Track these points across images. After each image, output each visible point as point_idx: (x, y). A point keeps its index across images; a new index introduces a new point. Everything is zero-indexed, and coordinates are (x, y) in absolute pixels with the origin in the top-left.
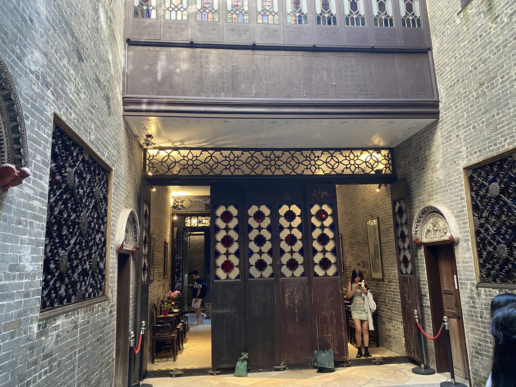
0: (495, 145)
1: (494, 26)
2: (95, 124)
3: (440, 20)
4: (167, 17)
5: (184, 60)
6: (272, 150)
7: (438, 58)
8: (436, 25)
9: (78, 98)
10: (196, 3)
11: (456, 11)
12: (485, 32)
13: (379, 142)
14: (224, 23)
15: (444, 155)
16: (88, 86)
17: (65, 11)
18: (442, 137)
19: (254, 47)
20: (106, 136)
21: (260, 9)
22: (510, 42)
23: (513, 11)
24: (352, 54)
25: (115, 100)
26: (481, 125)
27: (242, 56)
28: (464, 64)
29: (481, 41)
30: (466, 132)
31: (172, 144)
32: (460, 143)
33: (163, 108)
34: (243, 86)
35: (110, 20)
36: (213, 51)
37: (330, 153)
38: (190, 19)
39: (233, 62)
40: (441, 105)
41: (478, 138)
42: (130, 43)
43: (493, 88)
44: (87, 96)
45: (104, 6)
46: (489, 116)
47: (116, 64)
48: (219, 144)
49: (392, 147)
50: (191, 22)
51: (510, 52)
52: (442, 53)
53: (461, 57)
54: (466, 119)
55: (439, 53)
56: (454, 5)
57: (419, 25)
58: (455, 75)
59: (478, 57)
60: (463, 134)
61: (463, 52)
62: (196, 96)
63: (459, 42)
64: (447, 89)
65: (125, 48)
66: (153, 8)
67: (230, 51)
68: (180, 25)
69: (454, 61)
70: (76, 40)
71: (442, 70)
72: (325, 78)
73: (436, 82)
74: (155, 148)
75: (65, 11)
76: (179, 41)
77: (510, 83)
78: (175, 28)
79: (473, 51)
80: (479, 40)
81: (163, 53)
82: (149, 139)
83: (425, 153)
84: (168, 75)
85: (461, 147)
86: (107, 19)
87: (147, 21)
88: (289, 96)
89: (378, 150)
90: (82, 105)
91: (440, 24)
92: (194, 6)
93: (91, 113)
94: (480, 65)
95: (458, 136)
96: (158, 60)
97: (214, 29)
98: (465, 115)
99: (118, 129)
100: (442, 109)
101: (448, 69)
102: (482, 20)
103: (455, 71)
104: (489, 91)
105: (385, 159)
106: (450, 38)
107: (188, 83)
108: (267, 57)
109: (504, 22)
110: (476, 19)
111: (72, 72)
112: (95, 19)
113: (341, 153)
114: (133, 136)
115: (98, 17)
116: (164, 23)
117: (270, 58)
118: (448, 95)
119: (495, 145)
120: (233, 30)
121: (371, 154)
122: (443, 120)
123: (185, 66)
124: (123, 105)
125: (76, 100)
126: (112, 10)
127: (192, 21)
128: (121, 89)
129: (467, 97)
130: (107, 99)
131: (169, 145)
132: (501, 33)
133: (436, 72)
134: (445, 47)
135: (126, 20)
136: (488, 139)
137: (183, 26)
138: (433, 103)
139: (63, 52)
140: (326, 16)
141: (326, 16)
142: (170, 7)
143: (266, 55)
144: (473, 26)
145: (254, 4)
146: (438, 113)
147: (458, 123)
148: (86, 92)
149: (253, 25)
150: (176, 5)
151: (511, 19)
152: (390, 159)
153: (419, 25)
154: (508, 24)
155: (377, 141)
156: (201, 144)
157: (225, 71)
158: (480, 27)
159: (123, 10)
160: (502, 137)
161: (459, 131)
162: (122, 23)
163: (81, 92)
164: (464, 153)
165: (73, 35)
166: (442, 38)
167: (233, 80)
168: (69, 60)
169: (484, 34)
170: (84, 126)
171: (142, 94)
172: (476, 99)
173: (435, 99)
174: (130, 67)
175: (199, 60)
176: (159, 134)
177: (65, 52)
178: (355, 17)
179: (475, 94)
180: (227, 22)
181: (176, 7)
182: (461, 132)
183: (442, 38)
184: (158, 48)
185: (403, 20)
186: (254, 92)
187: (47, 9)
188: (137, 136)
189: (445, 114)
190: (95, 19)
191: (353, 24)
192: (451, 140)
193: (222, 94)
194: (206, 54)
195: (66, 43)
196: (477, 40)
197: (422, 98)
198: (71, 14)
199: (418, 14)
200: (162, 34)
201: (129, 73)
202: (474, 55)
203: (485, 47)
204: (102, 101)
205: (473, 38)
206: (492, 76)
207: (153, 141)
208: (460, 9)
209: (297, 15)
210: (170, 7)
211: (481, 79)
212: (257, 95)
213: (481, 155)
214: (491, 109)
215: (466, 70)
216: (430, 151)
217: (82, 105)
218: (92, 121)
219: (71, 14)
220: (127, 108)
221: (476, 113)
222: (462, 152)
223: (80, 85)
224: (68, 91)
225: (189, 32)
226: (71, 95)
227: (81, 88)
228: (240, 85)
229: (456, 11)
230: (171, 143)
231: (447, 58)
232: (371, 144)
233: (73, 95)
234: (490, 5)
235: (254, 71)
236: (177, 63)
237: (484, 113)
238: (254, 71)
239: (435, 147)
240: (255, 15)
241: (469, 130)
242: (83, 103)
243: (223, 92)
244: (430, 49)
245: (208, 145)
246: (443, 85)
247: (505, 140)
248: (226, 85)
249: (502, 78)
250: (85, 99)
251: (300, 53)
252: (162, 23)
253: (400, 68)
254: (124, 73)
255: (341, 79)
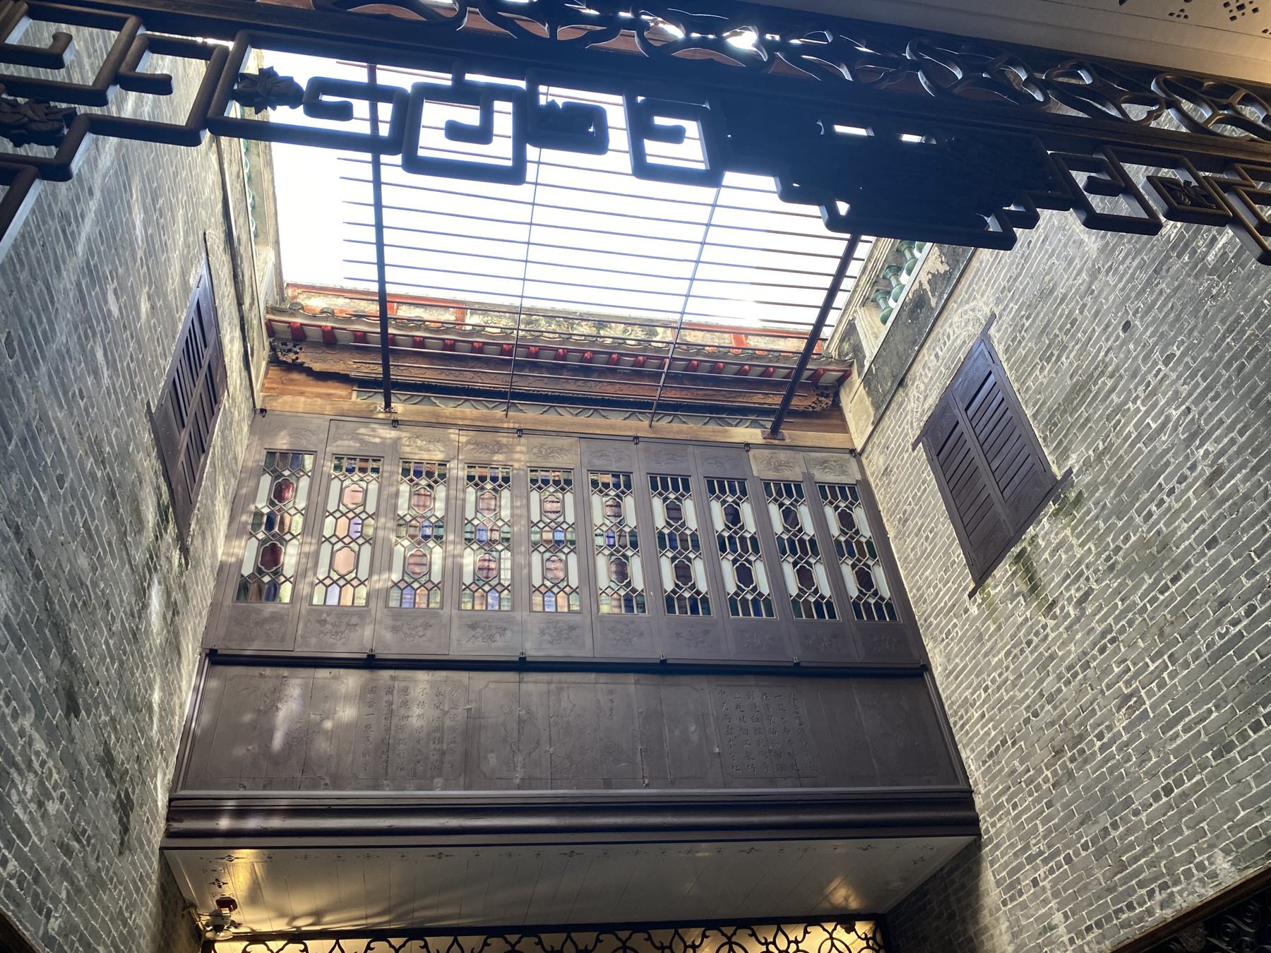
0: (1130, 907)
1: (1051, 623)
2: (72, 883)
3: (936, 606)
4: (317, 600)
5: (347, 698)
6: (568, 929)
7: (947, 688)
8: (929, 616)
9: (38, 816)
10: (390, 569)
11: (964, 590)
12: (1037, 634)
13: (846, 899)
14: (455, 612)
15: (1015, 936)
16: (76, 778)
17: (60, 600)
18: (998, 884)
19: (522, 666)
20: (95, 915)
21: (537, 581)
22: (1094, 658)
23: (1082, 593)
24: (751, 680)
25: (145, 808)
26: (1084, 854)
27: (492, 685)
28: (1007, 703)
29: (1032, 653)
30: (1051, 871)
31: (289, 924)
32: (1046, 902)
33: (276, 823)
34: (492, 759)
35: (173, 609)
36: (422, 676)
37: (723, 934)
38: (373, 605)
39: (469, 702)
40: (979, 802)
41: (1085, 888)
42: (215, 658)
43: (1086, 761)
44: (67, 806)
45: (164, 581)
46: (1096, 830)
47: (167, 710)
48: (423, 915)
49: (880, 912)
50: (373, 612)
51: (1100, 679)
52: (956, 678)
53: (999, 688)
54: (1045, 837)
55: (948, 676)
56: (958, 576)
57: (892, 616)
58: (995, 728)
59: (1034, 688)
60: (1046, 877)
61: (1000, 675)
62: (368, 788)
63: (986, 655)
64: (984, 762)
65: (200, 672)
66: (287, 580)
67: (463, 676)
68: (348, 617)
69: (983, 696)
70: (72, 664)
71: (962, 717)
72: (695, 738)
73: (956, 745)
74: (237, 938)
75: (60, 600)
76: (341, 650)
77: (1120, 749)
78: (334, 625)
79: (1020, 676)
80: (1027, 651)
81: (295, 684)
82: (226, 911)
83: (965, 931)
84: (302, 736)
85: (1049, 914)
86: (167, 607)
87: (269, 608)
88: (608, 784)
89: (847, 921)
90: (45, 832)
91: (937, 615)
92: (385, 576)
93: (68, 851)
94: (1042, 707)
95: (1035, 882)
96: (279, 699)
97: (427, 626)
98: (1040, 826)
99: (137, 890)
100: (982, 811)
101: (976, 715)
102: (1023, 611)
103: (991, 719)
104: (1079, 769)
105: (868, 947)
106: (966, 644)
107: (351, 756)
108: (553, 687)
109: (1068, 614)
110: (1010, 607)
111: (39, 745)
112: (136, 609)
113: (754, 934)
114: (181, 905)
115: (145, 606)
116: (309, 612)
117: (560, 690)
118: (990, 776)
119: (1130, 907)
120: (473, 627)
121: (831, 934)
122: (991, 840)
123: (347, 713)
124: (168, 820)
125: (33, 820)
126: (184, 588)
127: (377, 608)
128: (170, 776)
129: (1032, 781)
130: (125, 807)
131: (280, 925)
132: (1071, 639)
133: (951, 720)
134: (957, 665)
135: (215, 607)
136: (1110, 890)
137: (354, 620)
138: (957, 795)
139: (26, 696)
140: (687, 595)
141: (687, 595)
142: (360, 546)
143: (550, 683)
144: (1007, 620)
145: (525, 571)
146: (975, 821)
147: (1027, 847)
148: (68, 796)
149: (519, 615)
150: (343, 572)
151: (1083, 610)
152: (881, 948)
153: (892, 616)
154: (1078, 619)
155: (842, 895)
156: (370, 921)
157: (448, 723)
158: (1022, 624)
159: (212, 585)
160: (1141, 885)
161: (1036, 869)
162: (205, 613)
163: (50, 797)
164: (1062, 929)
165: (66, 653)
166: (948, 644)
167: (465, 746)
168: (40, 716)
169: (1036, 640)
170: (36, 895)
171: (226, 787)
172: (1054, 785)
173: (962, 786)
174: (206, 718)
175: (386, 698)
176: (254, 897)
177: (35, 699)
178: (750, 597)
179: (1048, 773)
180: (459, 609)
181: (342, 577)
182: (1041, 872)
183: (948, 644)
184: (285, 672)
185: (856, 605)
186: (519, 774)
187: (12, 600)
188: (193, 905)
189: (993, 825)
190: (136, 609)
191: (746, 613)
192: (1021, 893)
193: (436, 781)
194: (403, 684)
195: (41, 674)
196: (1022, 651)
197: (929, 783)
198: (74, 605)
199: (886, 592)
200: (299, 638)
201: (199, 732)
202: (1024, 686)
203: (1044, 666)
204: (107, 815)
205: (1014, 647)
206: (1076, 733)
207: (235, 916)
208: (972, 586)
209: (622, 593)
210: (360, 546)
211: (1053, 739)
212: (526, 783)
213: (1103, 937)
214: (1097, 811)
215: (1016, 718)
216: (977, 922)
217: (45, 832)
218: (65, 873)
219: (74, 605)
220: (177, 826)
221: (1064, 821)
222: (1056, 927)
223: (55, 776)
224: (15, 798)
225: (368, 631)
226: (19, 810)
227: (55, 788)
228: (485, 758)
229: (964, 590)
230: (285, 920)
231: (967, 688)
232: (828, 905)
233: (25, 808)
234: (1031, 579)
235: (521, 721)
236: (327, 706)
237: (1082, 823)
238: (521, 721)
239: (986, 912)
240: (525, 593)
241: (1059, 866)
242: (49, 828)
243: (440, 776)
244: (926, 668)
245: (389, 922)
246: (973, 750)
247: (1151, 894)
248: (448, 758)
249: (1100, 736)
250: (59, 815)
251: (631, 678)
252: (303, 611)
253: (863, 709)
254: (186, 731)
255: (727, 742)
